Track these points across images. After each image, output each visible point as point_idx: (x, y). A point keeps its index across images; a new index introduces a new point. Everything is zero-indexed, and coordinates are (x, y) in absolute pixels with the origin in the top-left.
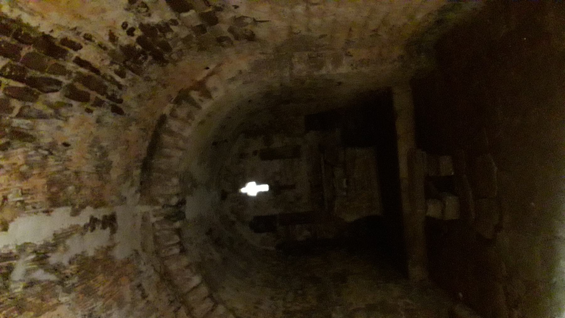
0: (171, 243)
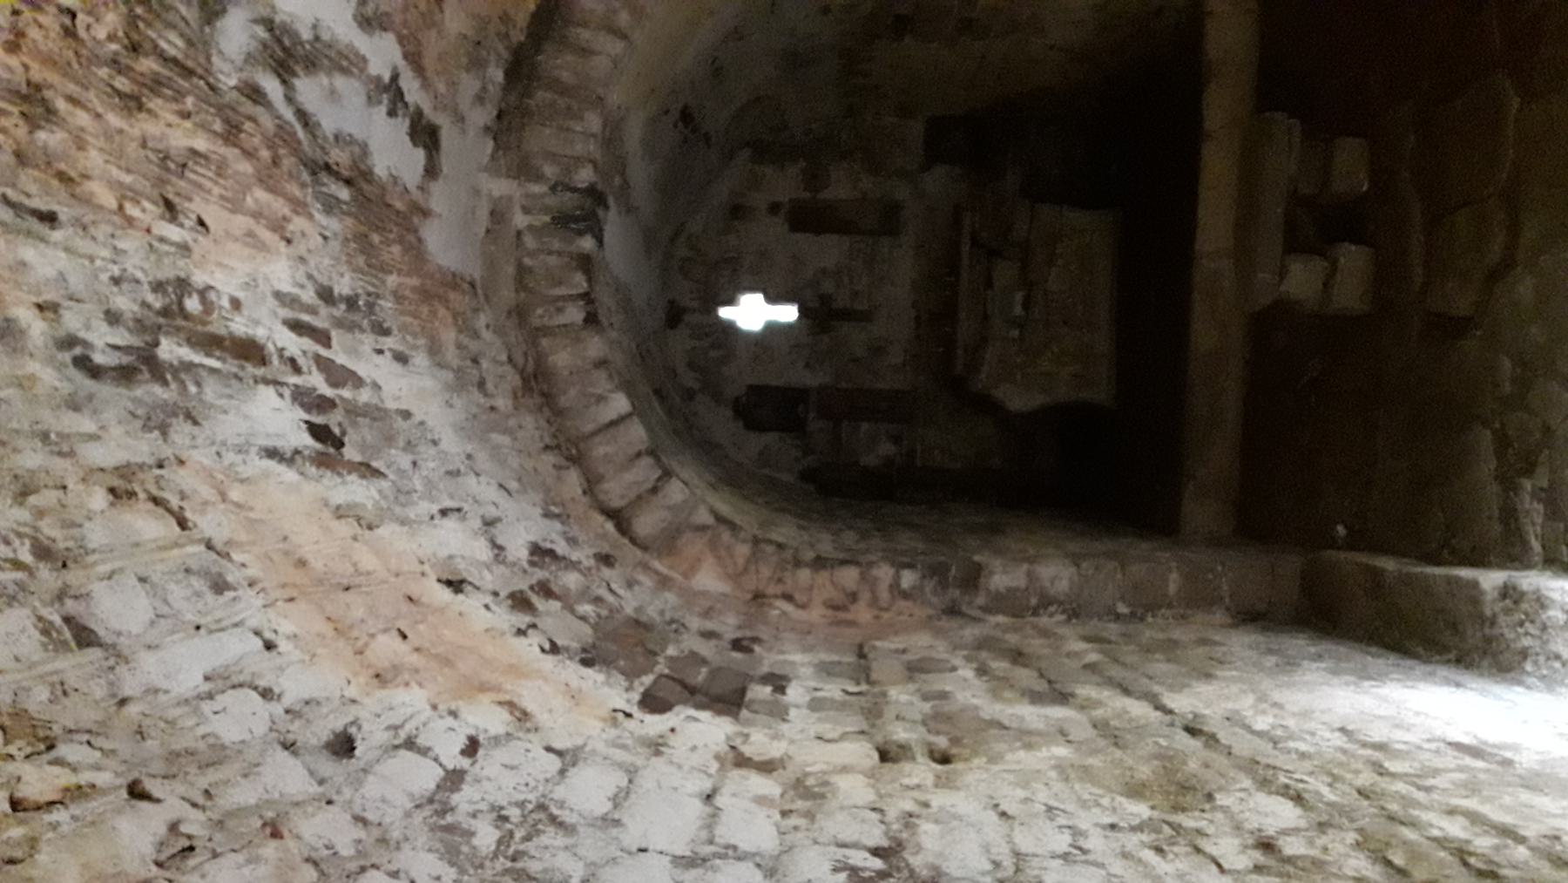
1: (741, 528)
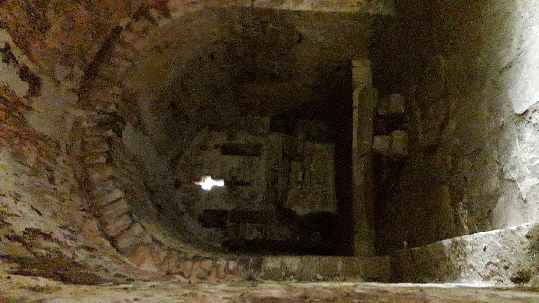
0: (99, 150)
1: (163, 244)
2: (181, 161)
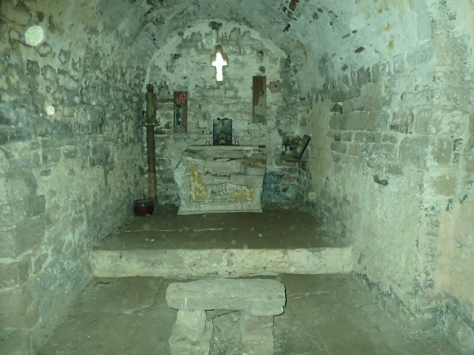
2: (244, 28)
